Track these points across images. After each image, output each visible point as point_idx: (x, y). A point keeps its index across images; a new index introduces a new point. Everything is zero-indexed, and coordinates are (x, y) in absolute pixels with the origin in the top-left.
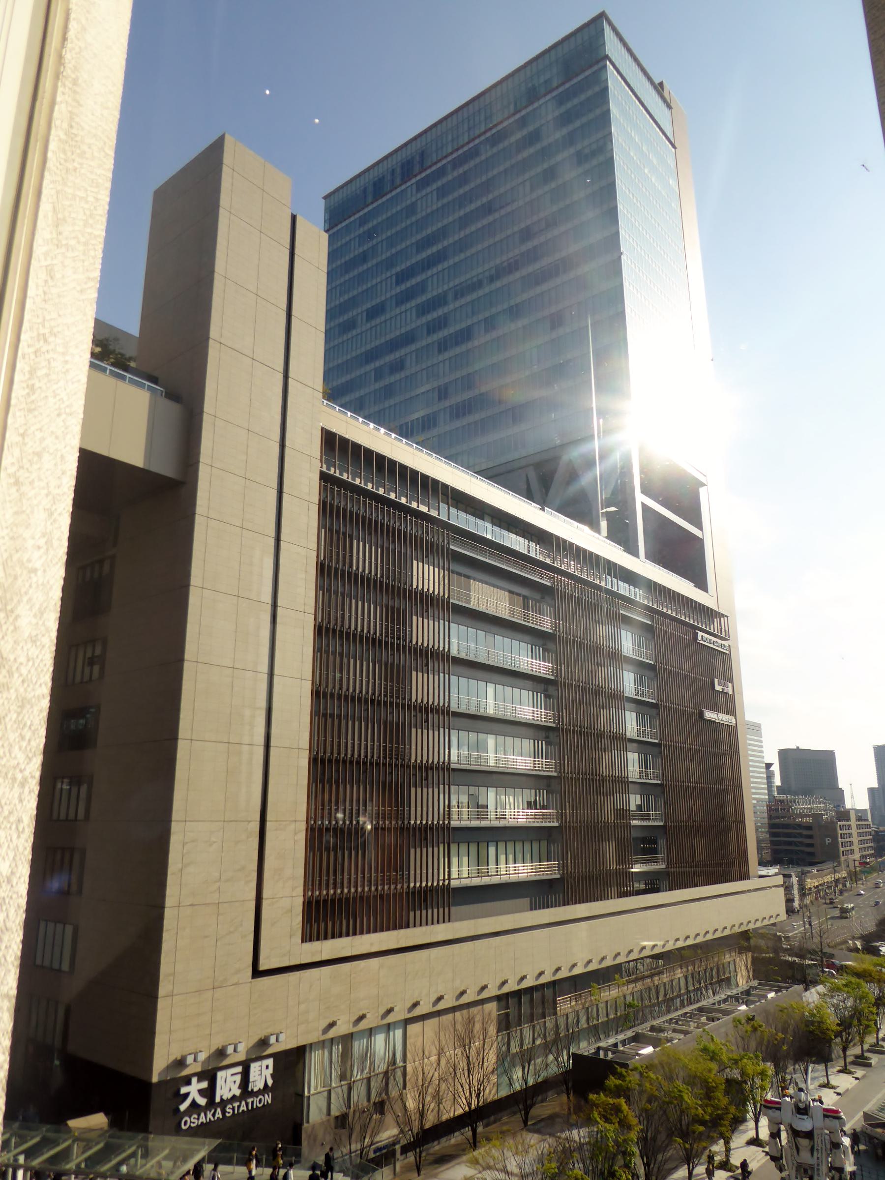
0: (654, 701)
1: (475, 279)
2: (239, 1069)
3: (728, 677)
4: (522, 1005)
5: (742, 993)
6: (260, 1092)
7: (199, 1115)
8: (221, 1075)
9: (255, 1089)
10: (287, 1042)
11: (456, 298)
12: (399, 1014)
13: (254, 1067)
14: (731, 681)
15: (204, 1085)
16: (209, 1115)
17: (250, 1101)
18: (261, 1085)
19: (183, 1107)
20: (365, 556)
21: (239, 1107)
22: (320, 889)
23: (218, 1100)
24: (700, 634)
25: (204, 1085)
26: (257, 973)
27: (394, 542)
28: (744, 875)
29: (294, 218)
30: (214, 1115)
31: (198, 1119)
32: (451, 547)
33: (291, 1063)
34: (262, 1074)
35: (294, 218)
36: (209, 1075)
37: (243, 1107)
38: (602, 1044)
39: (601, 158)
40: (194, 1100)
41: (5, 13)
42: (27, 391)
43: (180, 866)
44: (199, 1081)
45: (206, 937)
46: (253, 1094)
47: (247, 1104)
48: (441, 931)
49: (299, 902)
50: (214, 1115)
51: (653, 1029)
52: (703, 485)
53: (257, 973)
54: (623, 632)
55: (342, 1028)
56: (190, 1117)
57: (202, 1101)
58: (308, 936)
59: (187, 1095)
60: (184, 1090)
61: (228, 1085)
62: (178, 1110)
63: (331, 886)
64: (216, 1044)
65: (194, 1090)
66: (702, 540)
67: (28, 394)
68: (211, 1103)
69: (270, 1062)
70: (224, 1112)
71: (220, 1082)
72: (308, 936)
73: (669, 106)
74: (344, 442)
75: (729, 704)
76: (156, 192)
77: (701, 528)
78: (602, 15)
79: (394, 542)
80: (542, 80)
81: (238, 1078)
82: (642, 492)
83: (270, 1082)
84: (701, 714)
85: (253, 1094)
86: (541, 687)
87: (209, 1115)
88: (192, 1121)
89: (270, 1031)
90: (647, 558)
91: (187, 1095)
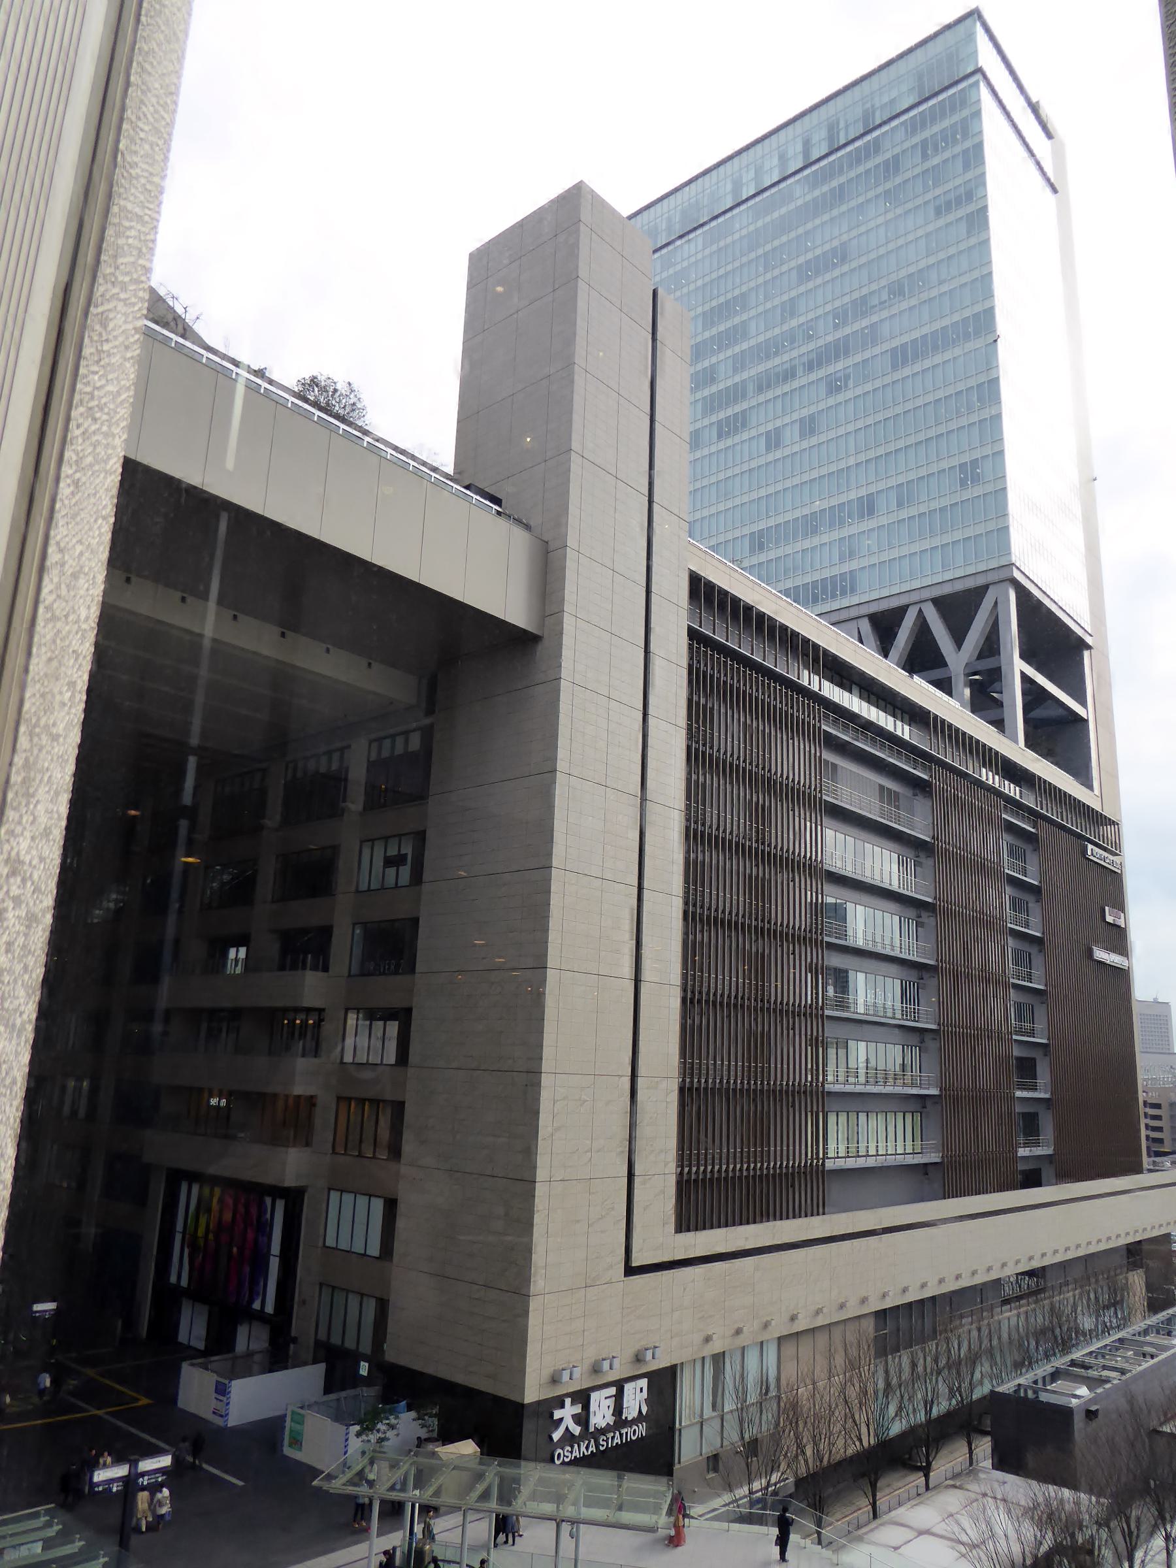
0: (1038, 934)
1: (787, 366)
2: (612, 1391)
3: (1119, 905)
4: (904, 1326)
5: (1162, 1323)
6: (635, 1421)
7: (572, 1447)
8: (595, 1397)
9: (630, 1418)
10: (662, 1362)
11: (760, 389)
12: (781, 1327)
13: (629, 1388)
14: (1123, 911)
15: (578, 1409)
16: (583, 1449)
17: (624, 1431)
18: (635, 1414)
19: (556, 1436)
20: (729, 736)
21: (613, 1438)
22: (690, 1166)
23: (592, 1429)
24: (1090, 847)
25: (578, 1409)
26: (631, 1270)
27: (757, 718)
28: (1137, 1169)
29: (655, 293)
30: (587, 1448)
31: (571, 1452)
32: (824, 727)
33: (663, 1383)
34: (636, 1399)
35: (655, 293)
36: (583, 1397)
37: (617, 1441)
38: (1022, 1381)
39: (971, 208)
40: (567, 1428)
41: (1035, 108)
42: (72, 488)
43: (550, 1129)
44: (573, 1403)
45: (578, 1221)
46: (626, 1423)
47: (621, 1435)
48: (816, 1226)
49: (672, 1180)
50: (587, 1448)
51: (1073, 1363)
52: (1089, 647)
53: (631, 1270)
54: (829, 833)
55: (716, 1347)
56: (563, 1449)
57: (576, 1430)
58: (683, 1225)
59: (561, 1420)
60: (557, 1414)
61: (601, 1413)
62: (551, 1439)
63: (738, 1160)
64: (591, 1355)
65: (567, 1413)
66: (1086, 721)
67: (73, 493)
68: (586, 1434)
69: (644, 1383)
70: (597, 1445)
71: (593, 1406)
72: (683, 1225)
73: (1049, 136)
74: (710, 586)
75: (1118, 939)
76: (472, 256)
77: (1083, 703)
78: (975, 14)
79: (757, 718)
80: (886, 99)
81: (611, 1402)
82: (1022, 657)
83: (644, 1410)
84: (1090, 953)
85: (626, 1423)
86: (911, 912)
87: (583, 1449)
88: (566, 1454)
89: (643, 1343)
90: (1026, 746)
91: (561, 1420)
